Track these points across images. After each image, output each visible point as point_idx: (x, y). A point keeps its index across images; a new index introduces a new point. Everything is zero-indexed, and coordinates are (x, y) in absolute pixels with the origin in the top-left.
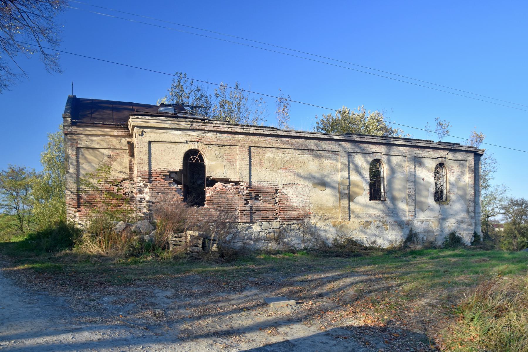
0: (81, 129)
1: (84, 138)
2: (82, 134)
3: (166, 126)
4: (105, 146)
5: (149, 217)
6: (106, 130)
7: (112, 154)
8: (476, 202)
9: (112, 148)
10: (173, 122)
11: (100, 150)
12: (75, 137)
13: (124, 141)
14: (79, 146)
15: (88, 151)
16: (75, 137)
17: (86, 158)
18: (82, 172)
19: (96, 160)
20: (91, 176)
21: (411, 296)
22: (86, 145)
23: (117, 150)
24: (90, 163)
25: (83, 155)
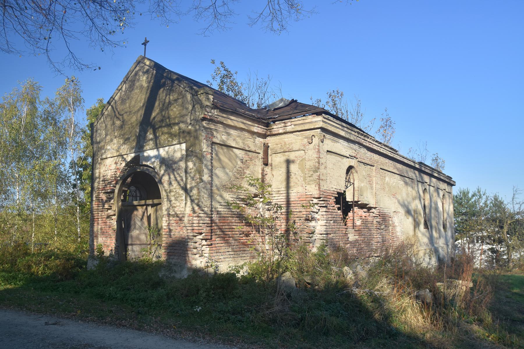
0: (224, 115)
1: (220, 127)
2: (222, 123)
3: (342, 133)
4: (241, 145)
5: (404, 262)
6: (248, 122)
7: (246, 158)
8: (212, 199)
9: (247, 149)
10: (350, 131)
11: (235, 150)
12: (212, 127)
13: (259, 141)
14: (215, 140)
15: (222, 149)
16: (212, 127)
17: (220, 160)
18: (216, 182)
19: (230, 164)
20: (86, 174)
21: (480, 321)
22: (223, 141)
23: (250, 153)
24: (224, 168)
25: (217, 155)
